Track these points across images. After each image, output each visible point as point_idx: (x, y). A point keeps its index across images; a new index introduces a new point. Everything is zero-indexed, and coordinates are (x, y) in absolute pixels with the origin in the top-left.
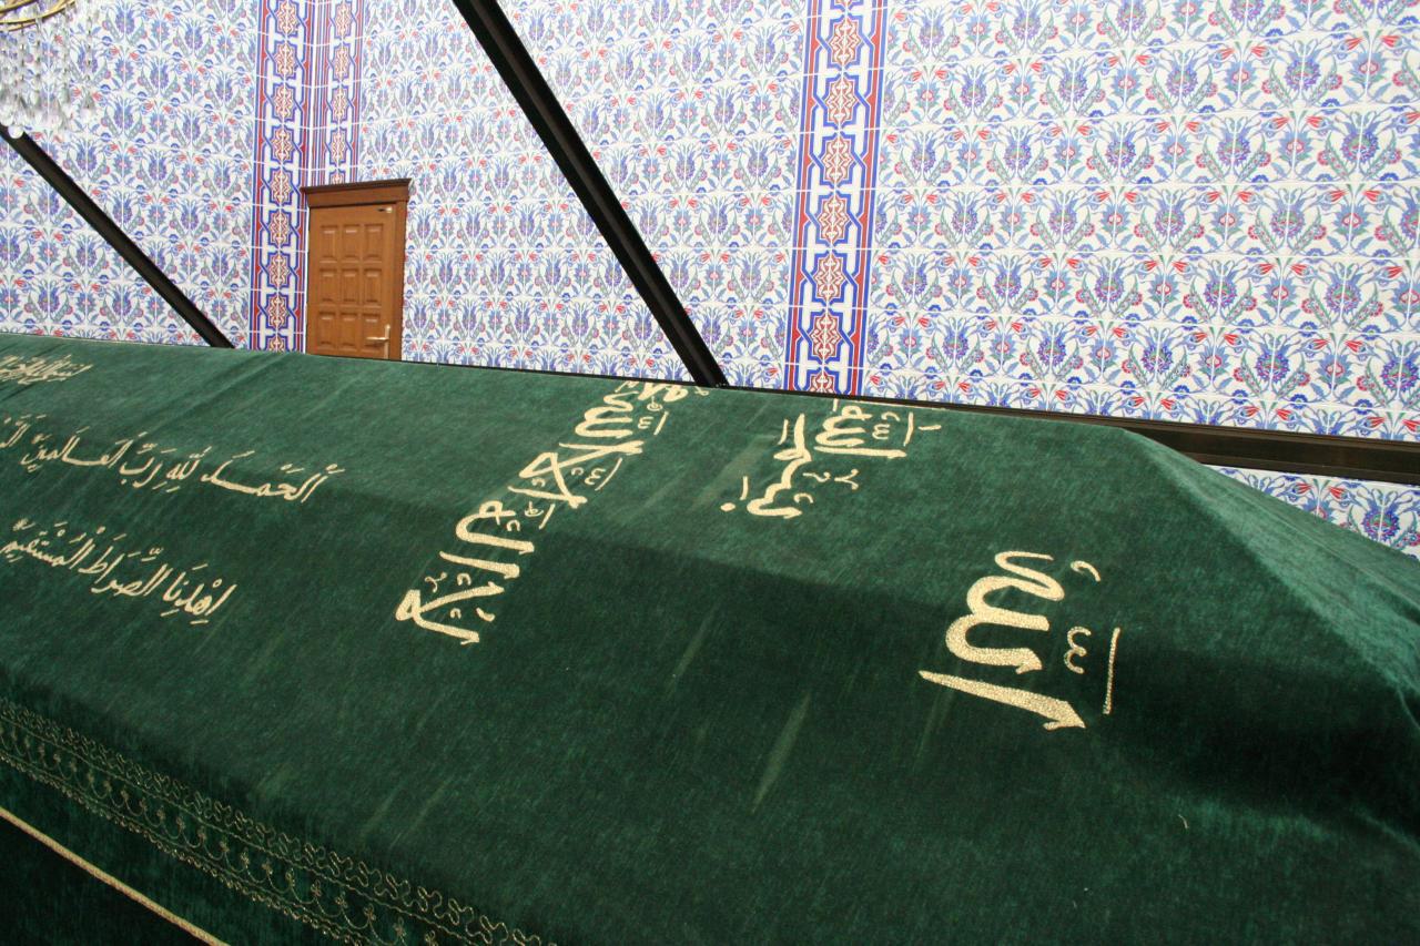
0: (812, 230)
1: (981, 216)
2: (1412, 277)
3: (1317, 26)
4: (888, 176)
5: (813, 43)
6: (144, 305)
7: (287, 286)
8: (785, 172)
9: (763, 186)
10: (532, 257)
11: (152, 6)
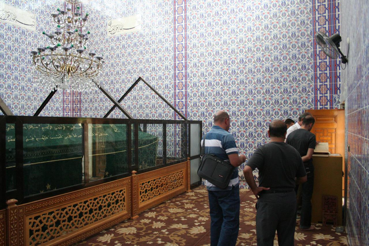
0: (177, 59)
1: (205, 74)
4: (189, 69)
5: (175, 67)
8: (171, 32)
9: (168, 72)
10: (119, 79)
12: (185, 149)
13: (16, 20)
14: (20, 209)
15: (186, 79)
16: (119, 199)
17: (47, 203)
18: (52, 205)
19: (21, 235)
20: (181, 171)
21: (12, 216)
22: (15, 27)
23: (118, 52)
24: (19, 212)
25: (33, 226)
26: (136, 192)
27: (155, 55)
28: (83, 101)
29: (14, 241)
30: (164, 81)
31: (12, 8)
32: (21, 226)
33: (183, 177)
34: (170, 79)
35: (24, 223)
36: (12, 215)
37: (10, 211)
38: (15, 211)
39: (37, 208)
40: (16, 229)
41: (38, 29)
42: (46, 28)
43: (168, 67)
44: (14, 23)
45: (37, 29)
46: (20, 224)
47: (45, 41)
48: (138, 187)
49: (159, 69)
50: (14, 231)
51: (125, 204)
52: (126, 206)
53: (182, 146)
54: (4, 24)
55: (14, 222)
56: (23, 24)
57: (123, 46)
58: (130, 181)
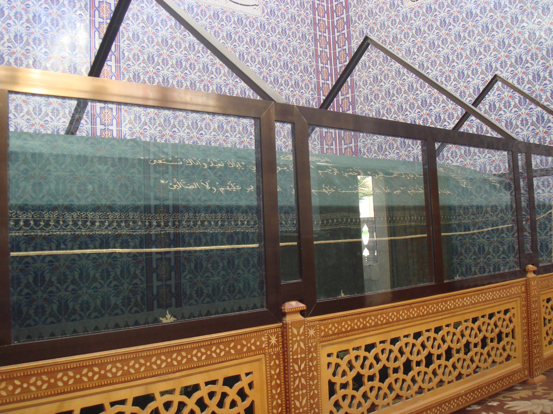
3: (507, 72)
6: (418, 86)
7: (158, 287)
11: (14, 4)
14: (310, 327)
22: (225, 12)
28: (362, 150)
37: (291, 328)
38: (301, 331)
39: (344, 330)
41: (266, 11)
42: (280, 9)
45: (263, 13)
47: (289, 21)
54: (206, 7)
55: (299, 357)
58: (523, 289)
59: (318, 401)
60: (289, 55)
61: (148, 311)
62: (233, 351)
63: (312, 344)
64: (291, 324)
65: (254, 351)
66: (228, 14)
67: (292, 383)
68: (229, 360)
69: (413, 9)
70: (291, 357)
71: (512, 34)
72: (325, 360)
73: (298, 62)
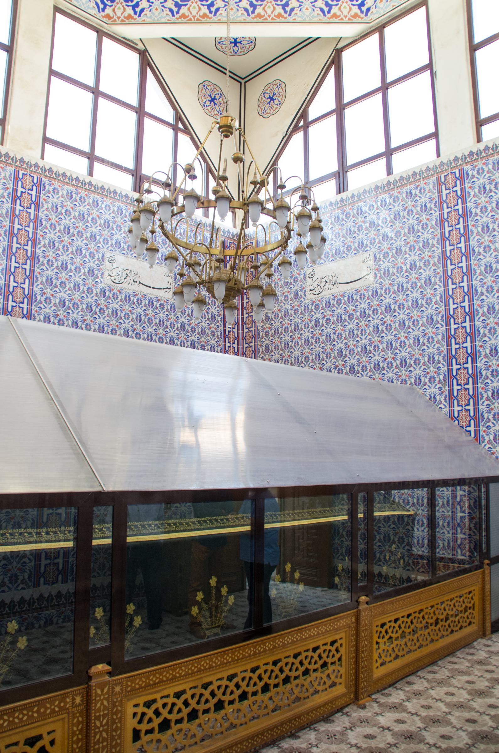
2: (496, 411)
12: (478, 537)
13: (138, 282)
14: (116, 685)
15: (475, 383)
16: (330, 660)
17: (171, 672)
18: (182, 676)
19: (116, 723)
20: (470, 592)
21: (99, 700)
22: (137, 295)
23: (328, 330)
24: (113, 692)
25: (140, 722)
26: (366, 645)
27: (405, 332)
29: (101, 723)
30: (426, 387)
31: (134, 261)
32: (117, 721)
33: (473, 605)
34: (439, 382)
35: (121, 715)
36: (98, 699)
37: (95, 690)
38: (105, 690)
40: (105, 727)
43: (434, 358)
44: (136, 288)
46: (115, 717)
48: (371, 633)
49: (415, 363)
50: (101, 733)
51: (343, 671)
52: (343, 676)
53: (470, 529)
54: (119, 291)
55: (102, 713)
56: (150, 287)
57: (340, 318)
58: (353, 619)
59: (120, 750)
60: (197, 336)
61: (34, 587)
62: (35, 715)
63: (117, 699)
64: (95, 686)
65: (57, 712)
66: (140, 297)
67: (93, 738)
68: (31, 723)
69: (314, 302)
70: (93, 715)
71: (399, 338)
72: (130, 710)
73: (205, 342)
